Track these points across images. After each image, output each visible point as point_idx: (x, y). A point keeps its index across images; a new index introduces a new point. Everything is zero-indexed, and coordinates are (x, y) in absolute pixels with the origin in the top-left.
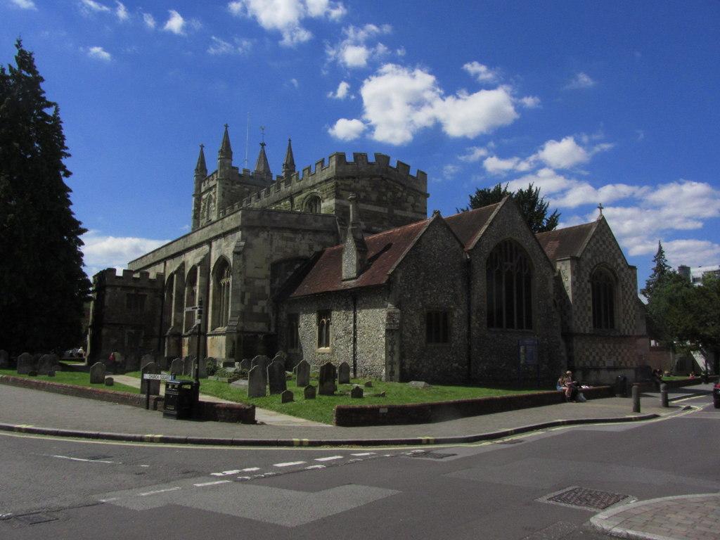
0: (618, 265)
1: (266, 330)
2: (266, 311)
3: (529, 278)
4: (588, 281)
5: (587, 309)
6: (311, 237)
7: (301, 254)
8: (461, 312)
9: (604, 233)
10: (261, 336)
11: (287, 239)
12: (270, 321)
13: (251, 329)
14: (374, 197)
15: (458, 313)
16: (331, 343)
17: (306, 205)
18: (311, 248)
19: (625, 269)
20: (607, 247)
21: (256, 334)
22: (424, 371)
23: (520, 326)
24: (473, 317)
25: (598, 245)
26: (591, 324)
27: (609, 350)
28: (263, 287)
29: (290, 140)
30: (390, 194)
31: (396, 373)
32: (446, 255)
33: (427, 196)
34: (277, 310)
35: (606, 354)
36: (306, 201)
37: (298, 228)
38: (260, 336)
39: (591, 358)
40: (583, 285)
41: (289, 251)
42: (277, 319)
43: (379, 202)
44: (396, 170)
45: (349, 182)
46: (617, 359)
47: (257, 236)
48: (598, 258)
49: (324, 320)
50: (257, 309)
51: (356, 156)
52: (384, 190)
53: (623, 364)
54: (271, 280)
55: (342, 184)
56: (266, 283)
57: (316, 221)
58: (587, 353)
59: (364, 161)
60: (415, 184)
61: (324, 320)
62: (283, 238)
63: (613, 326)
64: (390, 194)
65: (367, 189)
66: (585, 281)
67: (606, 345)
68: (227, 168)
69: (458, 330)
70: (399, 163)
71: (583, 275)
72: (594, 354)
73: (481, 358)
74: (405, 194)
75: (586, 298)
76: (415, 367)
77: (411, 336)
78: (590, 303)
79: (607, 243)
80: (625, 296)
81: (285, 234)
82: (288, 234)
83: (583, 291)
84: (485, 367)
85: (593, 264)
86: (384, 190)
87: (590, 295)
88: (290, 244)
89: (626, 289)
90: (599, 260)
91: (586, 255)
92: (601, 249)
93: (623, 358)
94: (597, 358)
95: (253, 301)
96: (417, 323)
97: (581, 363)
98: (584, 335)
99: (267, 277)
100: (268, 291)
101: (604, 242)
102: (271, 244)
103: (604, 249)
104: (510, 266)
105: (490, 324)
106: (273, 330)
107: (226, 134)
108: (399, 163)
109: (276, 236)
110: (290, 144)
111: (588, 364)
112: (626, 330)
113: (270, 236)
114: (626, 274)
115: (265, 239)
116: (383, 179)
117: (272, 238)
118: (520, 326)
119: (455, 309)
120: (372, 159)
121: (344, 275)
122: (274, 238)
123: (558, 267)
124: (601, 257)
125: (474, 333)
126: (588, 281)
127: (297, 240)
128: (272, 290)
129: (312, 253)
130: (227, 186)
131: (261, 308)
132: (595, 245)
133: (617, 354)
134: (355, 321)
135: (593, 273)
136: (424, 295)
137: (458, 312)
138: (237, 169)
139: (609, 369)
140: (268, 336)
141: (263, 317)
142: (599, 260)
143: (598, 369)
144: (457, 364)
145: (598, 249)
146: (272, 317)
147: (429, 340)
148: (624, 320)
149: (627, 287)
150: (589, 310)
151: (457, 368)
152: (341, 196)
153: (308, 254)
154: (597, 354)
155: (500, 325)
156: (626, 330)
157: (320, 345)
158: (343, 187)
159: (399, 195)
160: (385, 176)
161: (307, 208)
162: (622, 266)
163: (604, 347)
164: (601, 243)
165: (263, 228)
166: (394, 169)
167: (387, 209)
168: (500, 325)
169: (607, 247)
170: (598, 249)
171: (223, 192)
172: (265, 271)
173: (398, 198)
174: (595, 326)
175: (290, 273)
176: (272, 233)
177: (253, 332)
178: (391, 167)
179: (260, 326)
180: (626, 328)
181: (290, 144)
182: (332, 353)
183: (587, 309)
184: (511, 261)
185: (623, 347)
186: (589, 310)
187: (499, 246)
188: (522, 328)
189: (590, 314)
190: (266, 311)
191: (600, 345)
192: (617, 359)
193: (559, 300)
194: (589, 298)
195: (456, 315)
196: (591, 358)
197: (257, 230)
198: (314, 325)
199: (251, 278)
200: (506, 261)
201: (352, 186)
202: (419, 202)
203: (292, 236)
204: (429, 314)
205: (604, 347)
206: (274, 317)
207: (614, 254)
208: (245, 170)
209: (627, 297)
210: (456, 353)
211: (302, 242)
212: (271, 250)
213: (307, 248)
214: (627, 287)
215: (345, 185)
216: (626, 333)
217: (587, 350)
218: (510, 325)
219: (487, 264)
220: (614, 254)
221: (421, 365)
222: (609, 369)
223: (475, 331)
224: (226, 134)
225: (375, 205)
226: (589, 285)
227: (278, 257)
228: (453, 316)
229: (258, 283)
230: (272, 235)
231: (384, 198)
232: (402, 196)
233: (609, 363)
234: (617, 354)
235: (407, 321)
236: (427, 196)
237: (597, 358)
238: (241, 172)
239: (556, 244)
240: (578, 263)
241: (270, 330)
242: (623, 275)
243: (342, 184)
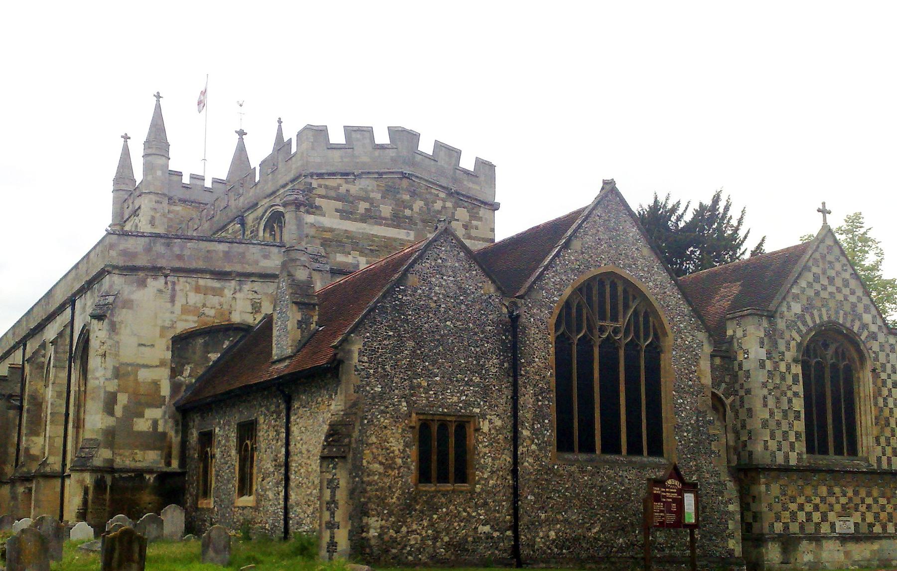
0: (865, 326)
1: (162, 466)
2: (160, 429)
3: (655, 352)
4: (795, 361)
5: (791, 416)
6: (257, 286)
7: (236, 318)
8: (498, 423)
9: (830, 263)
10: (150, 478)
11: (206, 291)
12: (170, 447)
13: (129, 463)
14: (386, 210)
15: (491, 424)
16: (254, 488)
17: (264, 230)
18: (256, 308)
19: (881, 337)
20: (839, 290)
21: (139, 473)
22: (412, 542)
23: (443, 426)
24: (526, 433)
25: (817, 287)
26: (801, 446)
27: (843, 500)
28: (156, 384)
29: (280, 122)
30: (418, 205)
31: (339, 549)
32: (463, 307)
33: (495, 207)
34: (184, 429)
35: (838, 507)
36: (263, 223)
37: (228, 269)
38: (147, 477)
39: (801, 516)
40: (783, 367)
41: (212, 312)
42: (184, 444)
43: (397, 221)
44: (433, 159)
45: (332, 182)
46: (864, 520)
47: (142, 284)
48: (815, 312)
49: (248, 442)
50: (142, 425)
51: (349, 131)
52: (407, 197)
53: (877, 529)
54: (173, 370)
55: (320, 186)
56: (165, 373)
57: (266, 257)
58: (793, 507)
59: (367, 141)
60: (471, 185)
61: (248, 442)
62: (198, 289)
63: (853, 451)
64: (418, 205)
65: (372, 195)
66: (789, 356)
67: (837, 490)
68: (159, 173)
69: (489, 460)
70: (438, 145)
71: (782, 347)
72: (808, 508)
73: (543, 516)
74: (449, 204)
75: (790, 394)
76: (392, 532)
77: (381, 470)
78: (799, 404)
79: (839, 282)
80: (880, 391)
81: (202, 282)
82: (206, 282)
83: (783, 378)
84: (552, 534)
85: (805, 323)
86: (407, 197)
87: (800, 388)
88: (214, 300)
89: (884, 376)
90: (820, 317)
91: (789, 308)
92: (824, 295)
93: (877, 517)
94: (816, 517)
95: (135, 411)
96: (396, 445)
97: (778, 527)
98: (786, 469)
99: (162, 364)
100: (165, 390)
101: (831, 280)
102: (173, 300)
103: (831, 293)
104: (610, 330)
105: (564, 443)
106: (175, 464)
107: (158, 108)
108: (438, 145)
109: (183, 284)
110: (280, 127)
111: (794, 528)
112: (884, 459)
113: (170, 286)
114: (882, 346)
115: (160, 291)
116: (404, 176)
117: (174, 290)
118: (443, 426)
119: (483, 416)
120: (382, 137)
121: (276, 353)
122: (177, 288)
123: (730, 332)
124: (824, 310)
125: (528, 463)
126: (795, 361)
127: (226, 291)
128: (176, 388)
129: (259, 317)
130: (160, 206)
131: (150, 422)
132: (810, 285)
133: (863, 508)
134: (287, 444)
135: (805, 343)
136: (412, 388)
137: (490, 422)
138: (180, 174)
139: (844, 539)
140: (163, 477)
141: (156, 440)
142: (820, 317)
143: (817, 538)
144: (487, 529)
145: (817, 293)
146: (175, 439)
147: (424, 476)
148: (877, 439)
149: (884, 371)
150: (797, 417)
151: (489, 536)
152: (318, 208)
153: (250, 319)
154: (816, 508)
155: (612, 446)
156: (884, 459)
157: (241, 493)
158: (322, 191)
159: (438, 205)
160: (407, 171)
161: (267, 235)
162: (873, 328)
163: (831, 493)
164: (825, 282)
165: (155, 270)
166: (426, 156)
167: (412, 233)
168: (587, 446)
169: (839, 290)
170: (817, 293)
171: (153, 218)
172: (162, 351)
173: (439, 212)
174: (810, 449)
175: (214, 357)
176: (176, 279)
177: (133, 471)
178: (421, 154)
179: (150, 458)
180: (884, 454)
181: (280, 127)
182: (256, 508)
183: (791, 416)
184: (615, 318)
185: (875, 493)
186: (797, 417)
187: (584, 289)
188: (640, 452)
189: (800, 426)
190: (160, 429)
191: (823, 490)
192: (864, 520)
193: (732, 398)
194: (796, 394)
195: (485, 427)
196: (801, 516)
197: (141, 274)
198: (233, 452)
199: (128, 365)
200: (603, 318)
201: (343, 190)
202: (480, 219)
203: (216, 284)
204: (424, 427)
205: (831, 493)
206: (179, 438)
207: (854, 306)
208: (193, 177)
209: (885, 392)
210: (486, 504)
211: (238, 295)
212: (172, 313)
213: (250, 309)
214: (884, 371)
215: (326, 187)
216: (885, 466)
217: (793, 499)
218: (612, 446)
219: (557, 325)
220: (854, 306)
221: (404, 529)
222: (844, 539)
223: (531, 460)
224: (158, 108)
225: (388, 226)
226: (797, 369)
227: (189, 323)
228: (478, 430)
229: (144, 375)
230: (174, 283)
231: (408, 212)
232: (444, 207)
233: (845, 526)
234: (863, 508)
235: (373, 439)
236: (495, 207)
237: (816, 517)
238: (186, 180)
239: (736, 289)
240: (770, 323)
241: (169, 464)
242: (875, 347)
243: (320, 186)
